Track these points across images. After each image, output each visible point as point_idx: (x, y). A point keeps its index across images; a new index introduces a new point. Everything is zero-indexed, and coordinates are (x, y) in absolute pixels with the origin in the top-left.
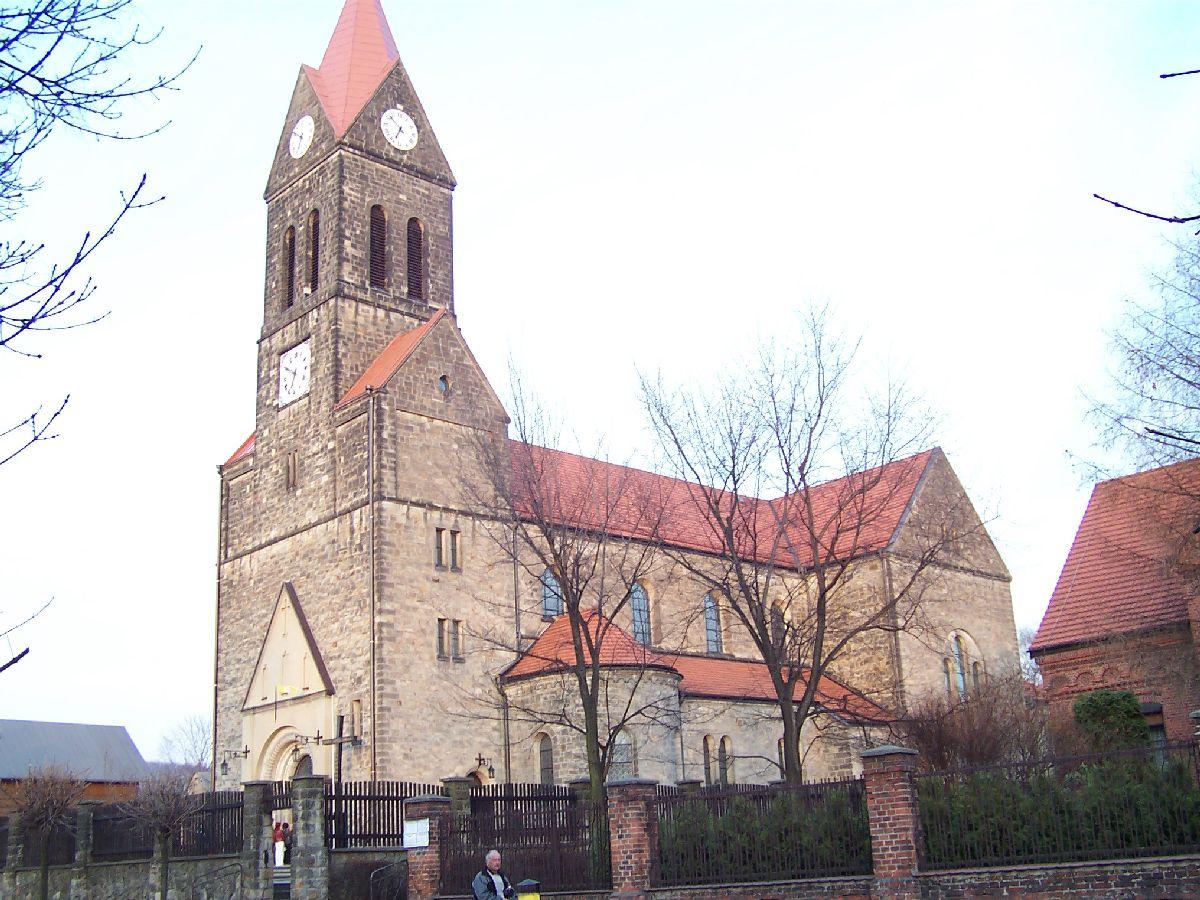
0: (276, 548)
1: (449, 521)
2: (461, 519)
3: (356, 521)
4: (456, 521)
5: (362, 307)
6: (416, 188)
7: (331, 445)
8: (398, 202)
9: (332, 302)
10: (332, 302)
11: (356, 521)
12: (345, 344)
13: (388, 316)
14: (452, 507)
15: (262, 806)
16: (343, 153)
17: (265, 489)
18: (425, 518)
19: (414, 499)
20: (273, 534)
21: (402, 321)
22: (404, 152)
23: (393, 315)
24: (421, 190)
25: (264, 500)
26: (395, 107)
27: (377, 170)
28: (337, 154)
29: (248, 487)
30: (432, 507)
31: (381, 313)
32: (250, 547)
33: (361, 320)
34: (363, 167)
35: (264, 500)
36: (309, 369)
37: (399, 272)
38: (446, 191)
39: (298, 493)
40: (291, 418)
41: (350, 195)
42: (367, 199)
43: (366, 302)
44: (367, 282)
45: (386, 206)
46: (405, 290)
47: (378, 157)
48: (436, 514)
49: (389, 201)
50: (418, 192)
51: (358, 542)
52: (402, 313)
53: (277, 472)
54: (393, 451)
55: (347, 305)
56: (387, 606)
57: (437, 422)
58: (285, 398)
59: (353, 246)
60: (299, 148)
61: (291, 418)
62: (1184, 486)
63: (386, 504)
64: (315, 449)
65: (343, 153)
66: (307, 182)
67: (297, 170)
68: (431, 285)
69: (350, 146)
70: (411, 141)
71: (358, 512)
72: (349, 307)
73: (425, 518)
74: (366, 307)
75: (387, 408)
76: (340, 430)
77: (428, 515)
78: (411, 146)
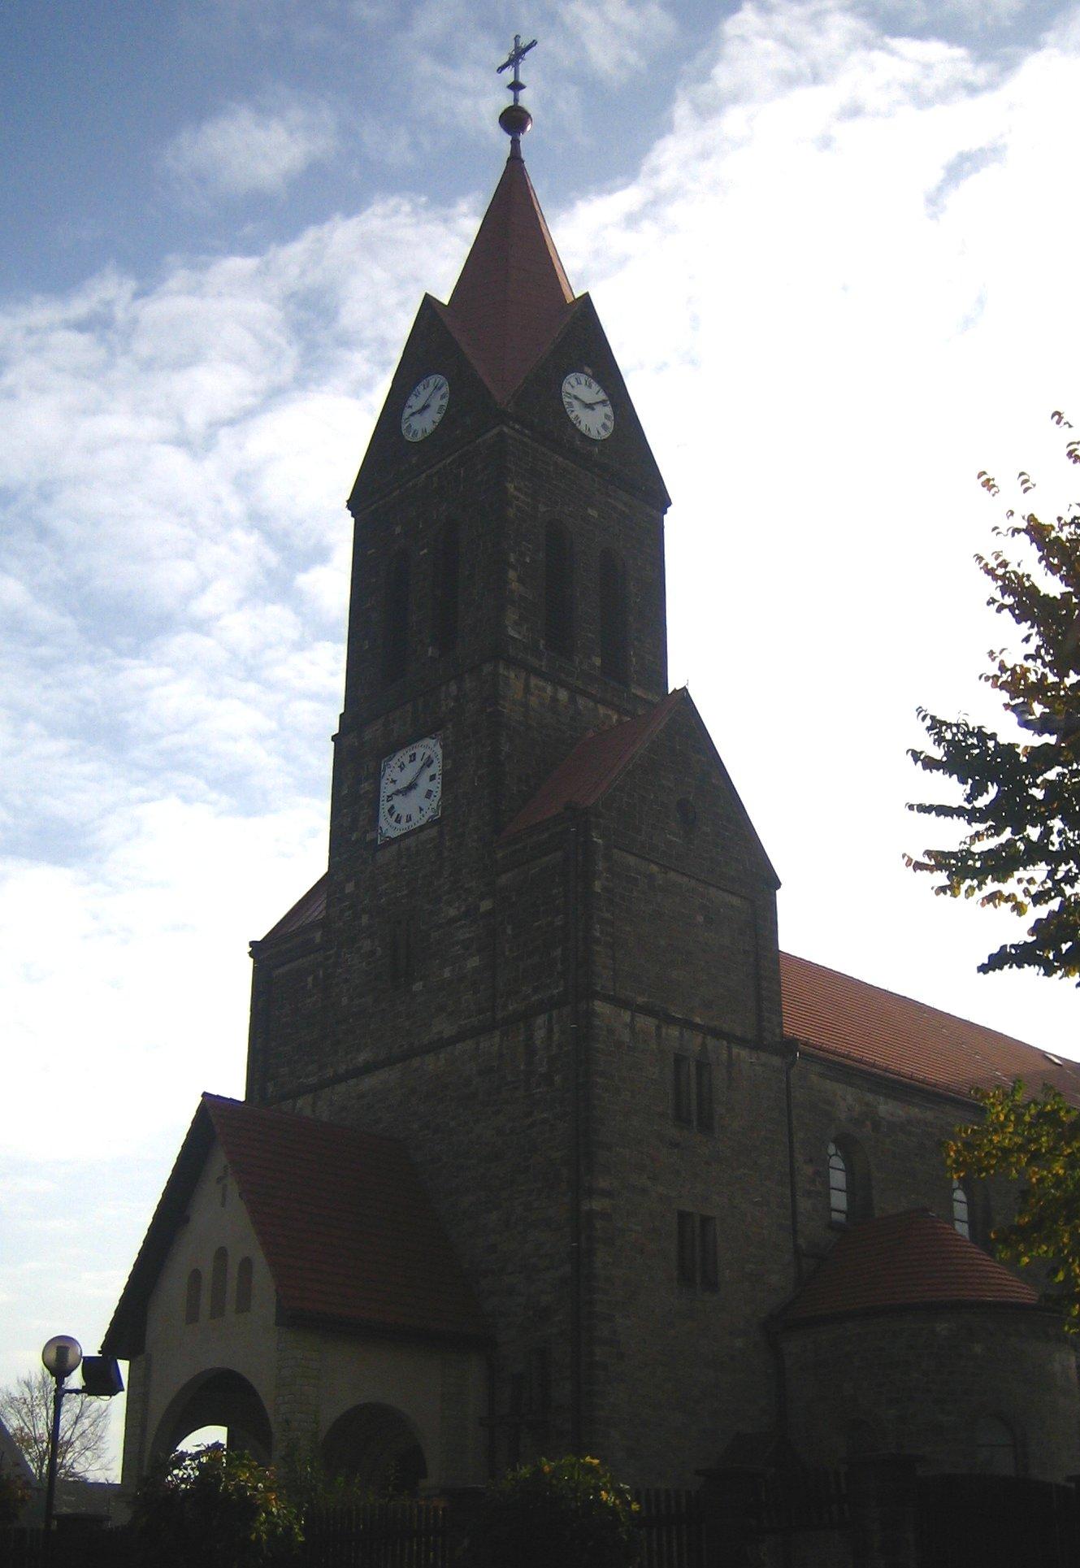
0: (369, 1082)
1: (695, 1042)
2: (711, 1042)
3: (540, 1034)
4: (704, 1045)
5: (534, 681)
7: (486, 905)
9: (487, 668)
10: (487, 668)
11: (540, 1034)
13: (572, 700)
14: (698, 1020)
15: (120, 1529)
16: (506, 429)
17: (346, 981)
18: (659, 1035)
19: (640, 1000)
20: (362, 1058)
25: (345, 1001)
26: (582, 372)
28: (495, 431)
29: (310, 979)
30: (670, 1020)
31: (563, 695)
32: (312, 1080)
33: (534, 701)
35: (345, 1001)
36: (439, 779)
39: (418, 986)
40: (404, 862)
41: (517, 499)
42: (542, 509)
43: (539, 674)
44: (542, 642)
46: (598, 661)
48: (674, 1032)
51: (543, 1070)
52: (589, 696)
53: (373, 953)
54: (608, 915)
55: (512, 675)
56: (603, 1184)
57: (672, 875)
58: (390, 828)
59: (520, 580)
60: (420, 425)
61: (404, 862)
62: (978, 1096)
63: (600, 1006)
64: (452, 912)
65: (506, 429)
66: (435, 479)
67: (414, 460)
70: (604, 426)
71: (541, 1020)
72: (514, 682)
73: (659, 1035)
74: (541, 683)
75: (600, 841)
76: (503, 880)
77: (664, 1030)
78: (605, 435)
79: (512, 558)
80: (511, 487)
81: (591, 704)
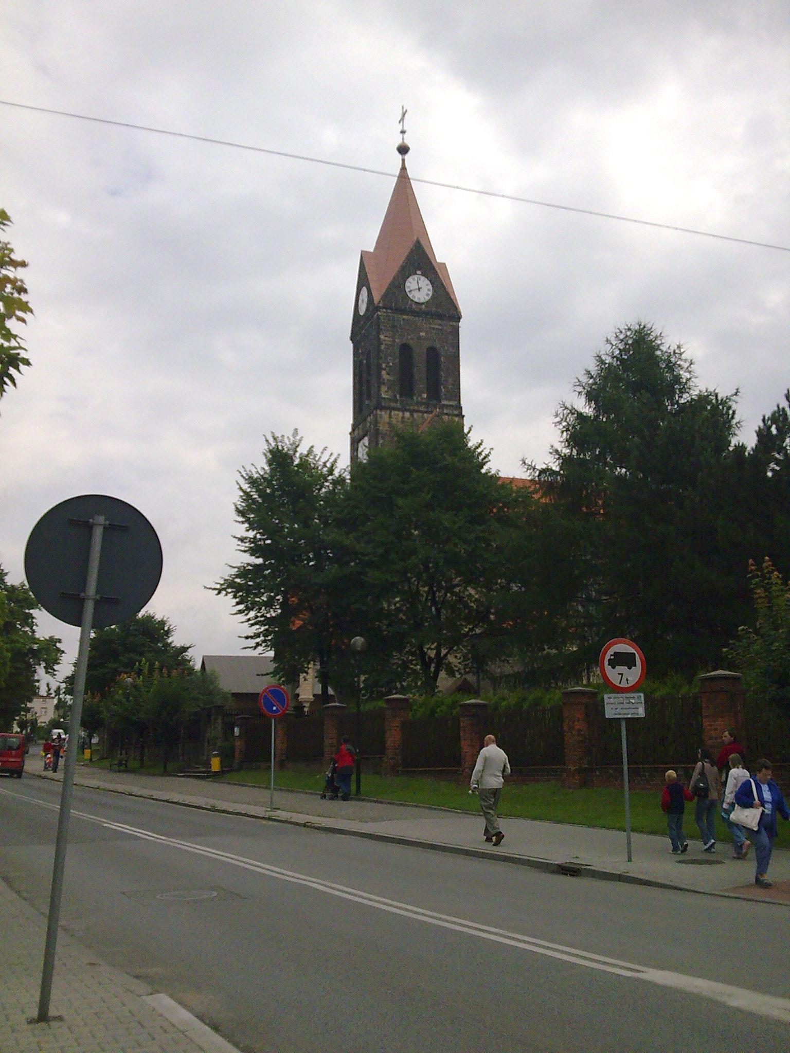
6: (432, 326)
12: (383, 438)
13: (412, 415)
21: (423, 417)
22: (423, 303)
23: (415, 415)
27: (403, 319)
37: (421, 384)
38: (454, 324)
43: (395, 409)
45: (411, 343)
68: (443, 390)
69: (383, 308)
74: (397, 412)
79: (384, 366)
80: (382, 337)
81: (421, 414)
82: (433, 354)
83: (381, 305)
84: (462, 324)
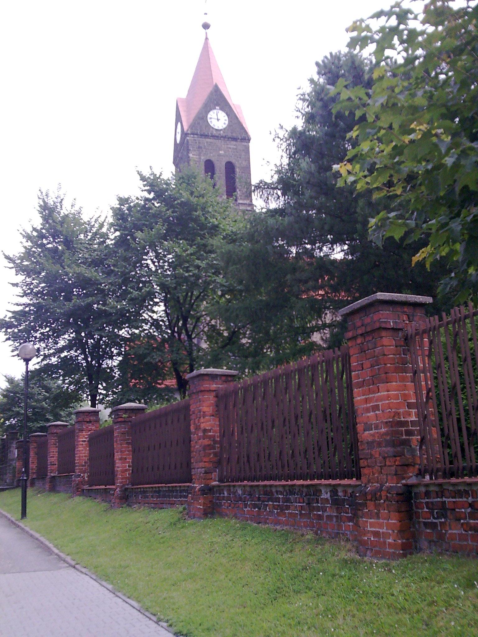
6: (229, 146)
8: (220, 155)
22: (221, 130)
24: (232, 147)
27: (207, 142)
34: (199, 143)
47: (206, 136)
49: (213, 156)
50: (230, 148)
80: (191, 155)
82: (230, 168)
83: (189, 132)
84: (252, 145)
